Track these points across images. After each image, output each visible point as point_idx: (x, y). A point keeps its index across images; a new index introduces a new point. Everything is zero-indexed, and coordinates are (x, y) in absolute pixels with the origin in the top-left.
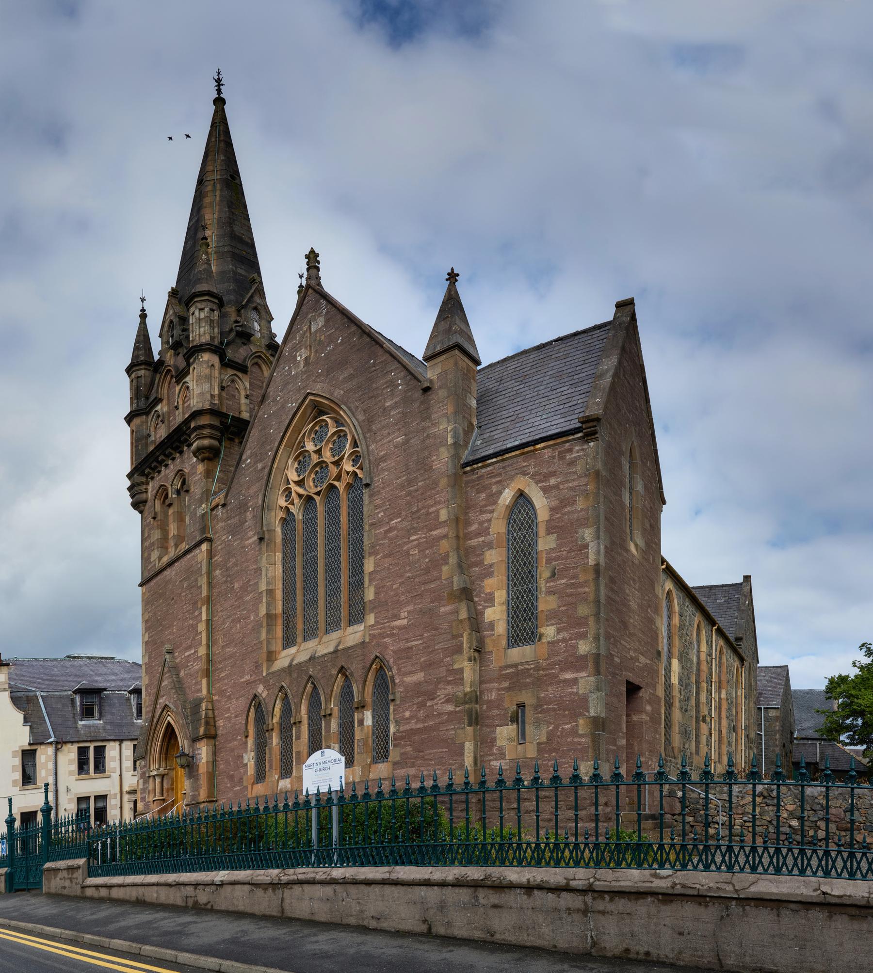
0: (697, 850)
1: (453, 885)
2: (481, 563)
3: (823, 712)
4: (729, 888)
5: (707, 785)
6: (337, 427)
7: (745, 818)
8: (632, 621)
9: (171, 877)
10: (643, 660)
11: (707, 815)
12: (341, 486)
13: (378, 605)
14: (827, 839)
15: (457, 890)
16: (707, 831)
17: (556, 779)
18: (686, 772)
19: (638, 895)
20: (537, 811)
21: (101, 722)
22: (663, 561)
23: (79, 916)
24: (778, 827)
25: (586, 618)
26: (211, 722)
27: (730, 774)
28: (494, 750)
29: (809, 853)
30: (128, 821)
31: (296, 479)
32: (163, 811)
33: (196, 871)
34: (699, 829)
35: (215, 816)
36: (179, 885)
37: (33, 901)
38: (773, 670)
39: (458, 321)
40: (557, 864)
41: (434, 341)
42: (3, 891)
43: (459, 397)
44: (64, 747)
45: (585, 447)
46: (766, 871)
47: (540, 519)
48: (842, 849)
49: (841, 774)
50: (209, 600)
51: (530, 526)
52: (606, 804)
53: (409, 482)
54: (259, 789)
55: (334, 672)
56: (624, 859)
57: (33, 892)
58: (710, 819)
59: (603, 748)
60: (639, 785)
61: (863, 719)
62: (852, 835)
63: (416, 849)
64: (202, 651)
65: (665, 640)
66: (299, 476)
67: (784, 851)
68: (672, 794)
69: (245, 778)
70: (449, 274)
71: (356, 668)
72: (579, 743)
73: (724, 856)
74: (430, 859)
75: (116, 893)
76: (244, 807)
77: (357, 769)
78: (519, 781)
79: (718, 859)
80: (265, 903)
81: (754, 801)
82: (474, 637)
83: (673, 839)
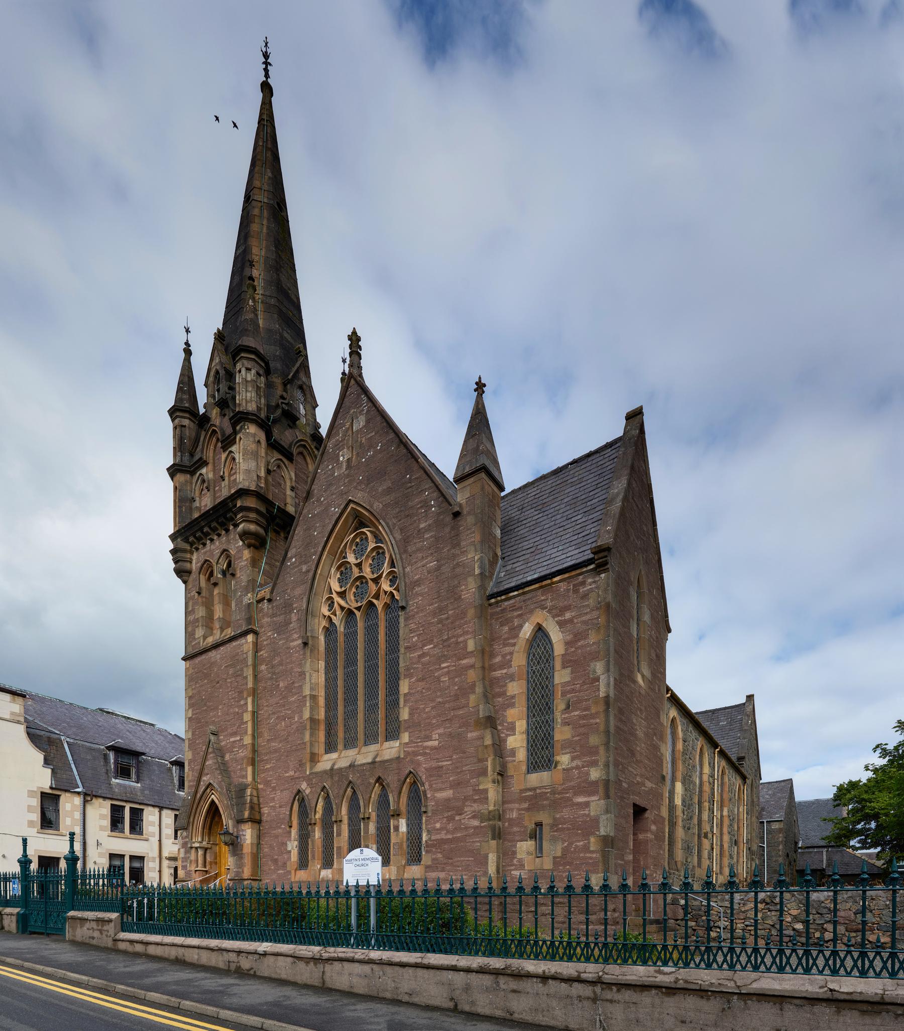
0: (700, 950)
1: (477, 972)
2: (503, 694)
3: (831, 820)
4: (732, 984)
5: (709, 894)
6: (376, 543)
7: (746, 923)
8: (638, 749)
9: (214, 943)
10: (649, 784)
11: (709, 920)
12: (379, 604)
13: (412, 725)
14: (834, 940)
15: (480, 976)
16: (709, 934)
17: (569, 888)
18: (689, 883)
19: (644, 987)
20: (553, 914)
21: (139, 785)
22: (668, 689)
23: (111, 967)
24: (781, 930)
25: (597, 747)
26: (255, 808)
27: (731, 884)
28: (515, 861)
29: (814, 953)
30: (167, 885)
31: (339, 590)
32: (206, 881)
33: (239, 940)
34: (701, 933)
35: (258, 893)
36: (221, 950)
37: (53, 945)
38: (776, 785)
39: (484, 440)
40: (570, 959)
41: (463, 461)
42: (15, 931)
43: (485, 525)
44: (94, 800)
45: (597, 579)
46: (768, 970)
47: (556, 654)
48: (852, 949)
49: (852, 879)
50: (254, 692)
51: (547, 660)
52: (614, 910)
53: (441, 610)
54: (302, 875)
55: (372, 781)
56: (630, 957)
57: (54, 937)
58: (712, 924)
59: (612, 862)
60: (644, 894)
61: (877, 822)
62: (863, 936)
63: (446, 940)
64: (248, 740)
65: (670, 766)
66: (341, 587)
67: (788, 952)
68: (675, 902)
69: (288, 863)
70: (477, 383)
71: (392, 779)
72: (591, 858)
73: (725, 956)
74: (457, 949)
75: (152, 950)
76: (287, 889)
77: (393, 869)
78: (536, 888)
79: (720, 959)
80: (307, 974)
81: (756, 907)
82: (498, 762)
83: (675, 941)
